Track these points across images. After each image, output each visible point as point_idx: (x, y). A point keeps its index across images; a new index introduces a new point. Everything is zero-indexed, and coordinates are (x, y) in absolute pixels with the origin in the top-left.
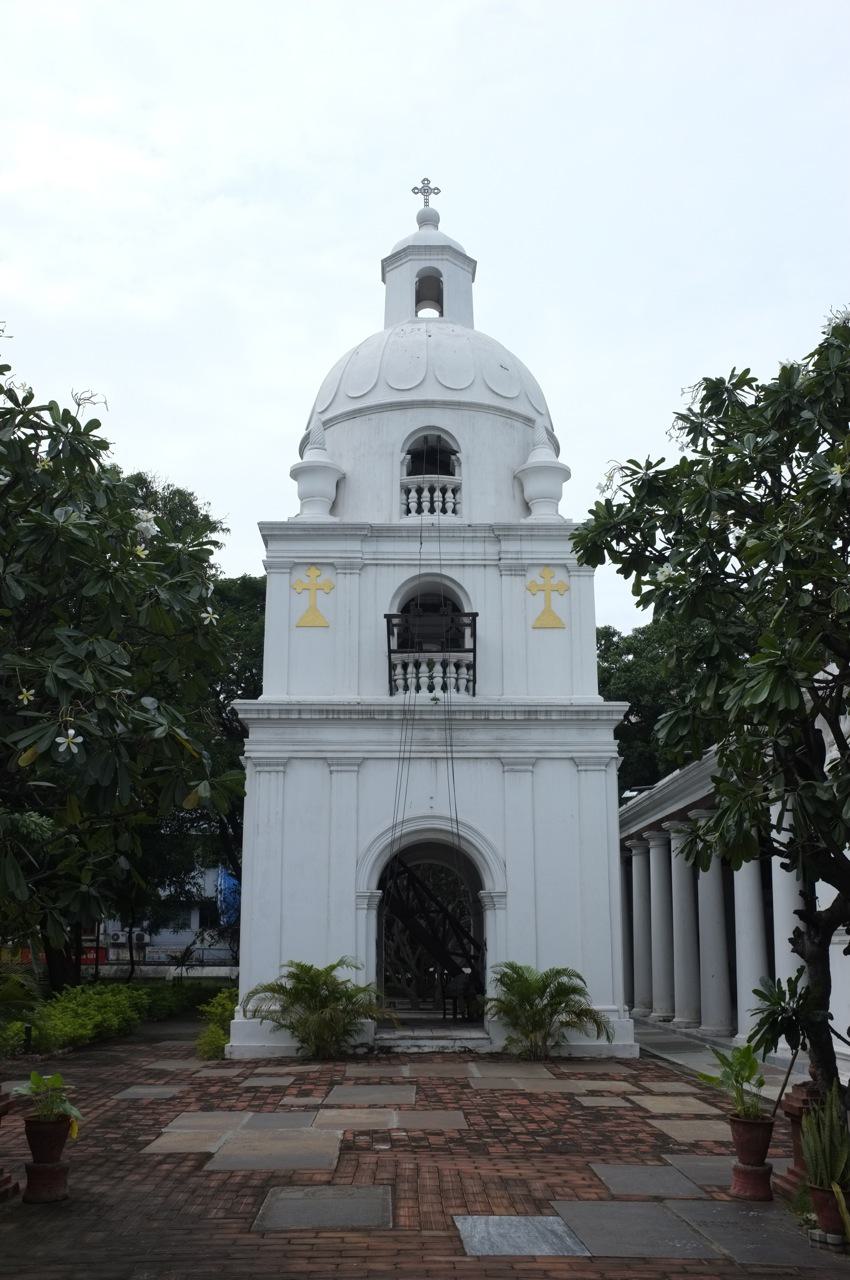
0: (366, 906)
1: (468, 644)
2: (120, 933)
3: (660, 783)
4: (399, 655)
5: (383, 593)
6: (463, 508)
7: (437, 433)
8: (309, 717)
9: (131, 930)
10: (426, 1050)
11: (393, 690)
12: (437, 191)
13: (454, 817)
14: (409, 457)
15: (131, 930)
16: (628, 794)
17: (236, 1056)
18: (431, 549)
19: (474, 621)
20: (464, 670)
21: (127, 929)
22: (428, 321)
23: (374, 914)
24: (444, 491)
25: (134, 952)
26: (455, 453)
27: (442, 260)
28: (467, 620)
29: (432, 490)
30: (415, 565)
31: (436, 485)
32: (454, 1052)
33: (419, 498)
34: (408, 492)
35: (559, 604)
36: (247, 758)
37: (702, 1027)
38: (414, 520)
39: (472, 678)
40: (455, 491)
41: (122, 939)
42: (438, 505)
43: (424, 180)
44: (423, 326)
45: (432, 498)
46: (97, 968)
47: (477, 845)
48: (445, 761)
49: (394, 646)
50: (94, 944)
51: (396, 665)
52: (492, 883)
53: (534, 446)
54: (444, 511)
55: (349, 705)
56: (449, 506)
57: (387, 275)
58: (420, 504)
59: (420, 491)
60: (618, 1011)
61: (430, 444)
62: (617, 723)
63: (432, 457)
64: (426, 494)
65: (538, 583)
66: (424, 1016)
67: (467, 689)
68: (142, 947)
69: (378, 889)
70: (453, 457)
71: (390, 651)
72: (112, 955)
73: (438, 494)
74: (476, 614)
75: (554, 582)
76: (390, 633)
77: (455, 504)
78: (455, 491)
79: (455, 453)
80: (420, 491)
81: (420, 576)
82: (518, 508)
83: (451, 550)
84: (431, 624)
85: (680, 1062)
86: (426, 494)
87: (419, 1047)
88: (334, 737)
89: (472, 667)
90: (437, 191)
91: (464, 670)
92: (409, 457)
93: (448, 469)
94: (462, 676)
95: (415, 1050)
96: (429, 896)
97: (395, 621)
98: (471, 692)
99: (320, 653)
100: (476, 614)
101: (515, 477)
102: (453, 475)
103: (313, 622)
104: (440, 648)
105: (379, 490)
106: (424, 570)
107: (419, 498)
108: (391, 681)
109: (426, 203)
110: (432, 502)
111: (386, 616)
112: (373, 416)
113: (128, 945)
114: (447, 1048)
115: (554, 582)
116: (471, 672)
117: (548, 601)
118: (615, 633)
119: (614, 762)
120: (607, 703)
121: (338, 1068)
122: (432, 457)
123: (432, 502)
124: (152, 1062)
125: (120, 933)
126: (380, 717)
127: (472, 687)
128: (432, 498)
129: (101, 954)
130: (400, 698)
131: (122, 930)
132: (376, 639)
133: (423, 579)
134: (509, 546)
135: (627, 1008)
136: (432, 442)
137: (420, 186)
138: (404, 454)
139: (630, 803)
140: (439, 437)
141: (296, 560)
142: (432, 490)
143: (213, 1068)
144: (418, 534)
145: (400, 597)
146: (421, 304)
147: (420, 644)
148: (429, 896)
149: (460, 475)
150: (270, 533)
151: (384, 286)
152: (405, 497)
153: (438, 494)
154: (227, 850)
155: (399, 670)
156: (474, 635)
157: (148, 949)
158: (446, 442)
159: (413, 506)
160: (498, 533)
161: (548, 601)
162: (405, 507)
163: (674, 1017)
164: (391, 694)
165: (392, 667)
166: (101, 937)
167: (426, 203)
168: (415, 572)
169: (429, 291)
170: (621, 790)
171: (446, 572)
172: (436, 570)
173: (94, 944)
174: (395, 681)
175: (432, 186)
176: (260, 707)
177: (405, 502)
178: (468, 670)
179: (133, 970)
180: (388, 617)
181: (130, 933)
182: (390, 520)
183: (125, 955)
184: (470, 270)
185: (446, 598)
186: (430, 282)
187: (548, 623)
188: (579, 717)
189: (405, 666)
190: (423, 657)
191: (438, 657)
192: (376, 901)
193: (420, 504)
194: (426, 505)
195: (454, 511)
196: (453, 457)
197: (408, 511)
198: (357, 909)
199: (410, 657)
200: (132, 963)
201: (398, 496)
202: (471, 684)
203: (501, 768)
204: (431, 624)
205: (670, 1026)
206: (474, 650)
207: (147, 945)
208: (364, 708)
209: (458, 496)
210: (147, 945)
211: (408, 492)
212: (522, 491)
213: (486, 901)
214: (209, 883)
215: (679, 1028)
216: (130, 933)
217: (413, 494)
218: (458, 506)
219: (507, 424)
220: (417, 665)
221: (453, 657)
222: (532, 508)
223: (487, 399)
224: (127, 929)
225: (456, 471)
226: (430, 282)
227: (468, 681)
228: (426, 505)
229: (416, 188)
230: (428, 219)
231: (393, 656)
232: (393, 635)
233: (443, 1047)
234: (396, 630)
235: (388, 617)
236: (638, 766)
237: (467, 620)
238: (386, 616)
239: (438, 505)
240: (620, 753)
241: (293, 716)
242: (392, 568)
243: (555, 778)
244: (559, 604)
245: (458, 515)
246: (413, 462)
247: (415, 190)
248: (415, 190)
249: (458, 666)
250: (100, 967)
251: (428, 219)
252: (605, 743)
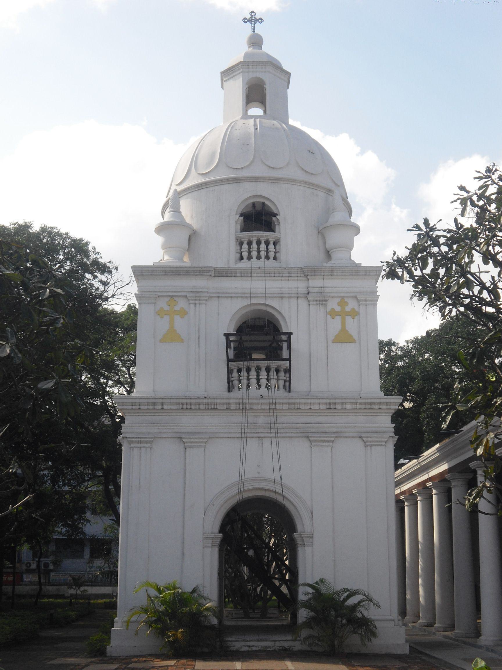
0: (210, 545)
1: (285, 354)
2: (32, 562)
3: (425, 454)
4: (235, 363)
5: (223, 317)
6: (282, 256)
7: (262, 200)
8: (169, 407)
9: (39, 559)
10: (254, 649)
11: (230, 388)
12: (260, 21)
13: (278, 478)
14: (242, 218)
15: (39, 559)
16: (402, 461)
17: (115, 654)
18: (258, 285)
19: (289, 338)
20: (282, 374)
21: (37, 559)
22: (255, 117)
23: (216, 550)
24: (267, 243)
25: (42, 575)
26: (275, 215)
27: (265, 72)
28: (284, 338)
29: (259, 243)
30: (247, 297)
31: (262, 239)
32: (275, 650)
33: (249, 248)
34: (241, 244)
35: (351, 324)
36: (123, 438)
37: (456, 631)
38: (245, 264)
39: (288, 379)
40: (275, 244)
41: (34, 566)
42: (263, 254)
43: (251, 12)
44: (252, 121)
45: (259, 248)
46: (14, 588)
47: (292, 500)
48: (269, 439)
49: (231, 356)
50: (12, 570)
51: (232, 370)
52: (304, 524)
53: (333, 210)
54: (267, 258)
55: (199, 398)
56: (272, 255)
57: (225, 83)
58: (250, 252)
59: (250, 243)
60: (393, 620)
61: (256, 208)
62: (393, 411)
63: (259, 218)
64: (254, 246)
65: (165, 309)
66: (254, 624)
67: (284, 387)
68: (48, 572)
69: (220, 533)
70: (274, 218)
71: (229, 360)
72: (27, 578)
73: (263, 246)
74: (291, 333)
75: (177, 308)
76: (228, 346)
77: (275, 253)
78: (275, 244)
79: (275, 215)
80: (250, 243)
81: (250, 305)
82: (322, 255)
83: (274, 285)
84: (258, 341)
85: (439, 657)
86: (254, 246)
87: (249, 646)
88: (188, 421)
89: (288, 371)
90: (260, 21)
91: (282, 374)
92: (242, 218)
93: (269, 227)
94: (281, 378)
95: (246, 649)
96: (256, 531)
97: (232, 338)
98: (288, 389)
99: (167, 368)
100: (291, 333)
101: (319, 233)
102: (273, 231)
103: (172, 337)
104: (266, 355)
105: (223, 241)
106: (253, 301)
107: (249, 248)
108: (229, 381)
109: (253, 29)
110: (259, 251)
111: (225, 335)
112: (216, 188)
113: (37, 571)
114: (270, 647)
115: (177, 308)
116: (287, 375)
117: (343, 323)
118: (394, 344)
119: (391, 439)
120: (386, 397)
121: (189, 663)
122: (259, 218)
123: (259, 251)
124: (54, 659)
125: (32, 562)
126: (221, 408)
127: (288, 387)
128: (259, 248)
129: (18, 579)
130: (236, 394)
131: (33, 560)
132: (218, 352)
133: (253, 308)
134: (316, 283)
135: (400, 618)
136: (258, 208)
137: (248, 17)
138: (238, 216)
139: (403, 468)
140: (263, 203)
141: (160, 294)
142: (259, 243)
143: (98, 663)
144: (246, 274)
145: (235, 322)
146: (248, 105)
147: (250, 355)
148: (256, 531)
149: (279, 232)
150: (140, 273)
151: (222, 92)
152: (239, 248)
153: (263, 246)
154: (110, 504)
155: (235, 374)
156: (289, 348)
157: (52, 574)
158: (269, 206)
159: (245, 254)
160: (307, 272)
161: (343, 323)
162: (238, 255)
163: (435, 623)
164: (229, 391)
165: (230, 372)
166: (18, 565)
167: (253, 29)
168: (246, 302)
169: (255, 94)
170: (397, 459)
171: (269, 302)
172: (262, 301)
173: (12, 570)
174: (232, 381)
175: (257, 17)
176: (133, 401)
177: (239, 251)
178: (285, 373)
179: (41, 589)
180: (227, 335)
181: (39, 562)
182: (228, 264)
183: (35, 578)
184: (286, 79)
185: (269, 322)
186: (260, 84)
187: (344, 337)
188: (368, 406)
189: (239, 371)
190: (253, 364)
191: (263, 364)
192: (218, 541)
193: (250, 252)
194: (254, 254)
195: (275, 258)
196: (274, 218)
197: (242, 258)
198: (204, 548)
199: (243, 364)
200: (40, 583)
201: (234, 247)
202: (287, 384)
203: (309, 444)
204: (258, 341)
205: (433, 629)
206: (289, 359)
207: (51, 570)
208: (210, 401)
209: (277, 247)
210: (51, 570)
211: (241, 244)
212: (325, 243)
213: (299, 541)
214: (94, 526)
215: (438, 631)
216: (39, 562)
217: (245, 246)
218: (277, 255)
219: (313, 193)
220: (248, 370)
221: (274, 364)
222: (332, 255)
223: (300, 175)
224: (37, 559)
225: (277, 227)
226: (260, 84)
227: (285, 381)
228: (254, 254)
229: (245, 18)
230: (256, 41)
231: (230, 363)
232: (230, 348)
233: (266, 647)
234: (232, 345)
235: (227, 335)
236: (409, 441)
237: (284, 338)
238: (225, 335)
239: (263, 254)
240: (396, 433)
241: (156, 405)
242: (229, 299)
243: (350, 451)
244: (351, 324)
245: (278, 261)
246: (244, 222)
247: (245, 20)
248: (245, 20)
249: (277, 371)
250: (16, 587)
251: (256, 41)
252: (385, 423)
